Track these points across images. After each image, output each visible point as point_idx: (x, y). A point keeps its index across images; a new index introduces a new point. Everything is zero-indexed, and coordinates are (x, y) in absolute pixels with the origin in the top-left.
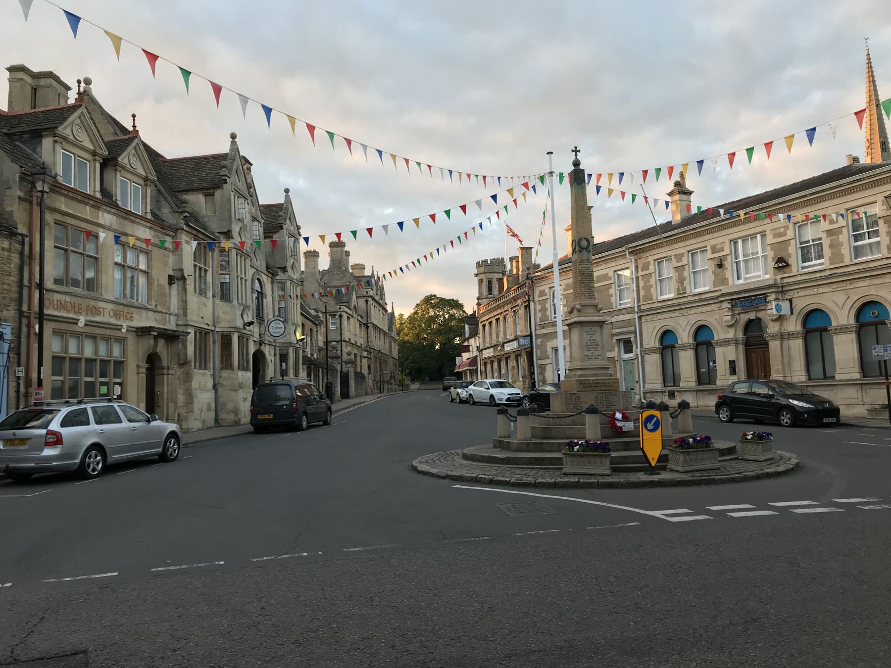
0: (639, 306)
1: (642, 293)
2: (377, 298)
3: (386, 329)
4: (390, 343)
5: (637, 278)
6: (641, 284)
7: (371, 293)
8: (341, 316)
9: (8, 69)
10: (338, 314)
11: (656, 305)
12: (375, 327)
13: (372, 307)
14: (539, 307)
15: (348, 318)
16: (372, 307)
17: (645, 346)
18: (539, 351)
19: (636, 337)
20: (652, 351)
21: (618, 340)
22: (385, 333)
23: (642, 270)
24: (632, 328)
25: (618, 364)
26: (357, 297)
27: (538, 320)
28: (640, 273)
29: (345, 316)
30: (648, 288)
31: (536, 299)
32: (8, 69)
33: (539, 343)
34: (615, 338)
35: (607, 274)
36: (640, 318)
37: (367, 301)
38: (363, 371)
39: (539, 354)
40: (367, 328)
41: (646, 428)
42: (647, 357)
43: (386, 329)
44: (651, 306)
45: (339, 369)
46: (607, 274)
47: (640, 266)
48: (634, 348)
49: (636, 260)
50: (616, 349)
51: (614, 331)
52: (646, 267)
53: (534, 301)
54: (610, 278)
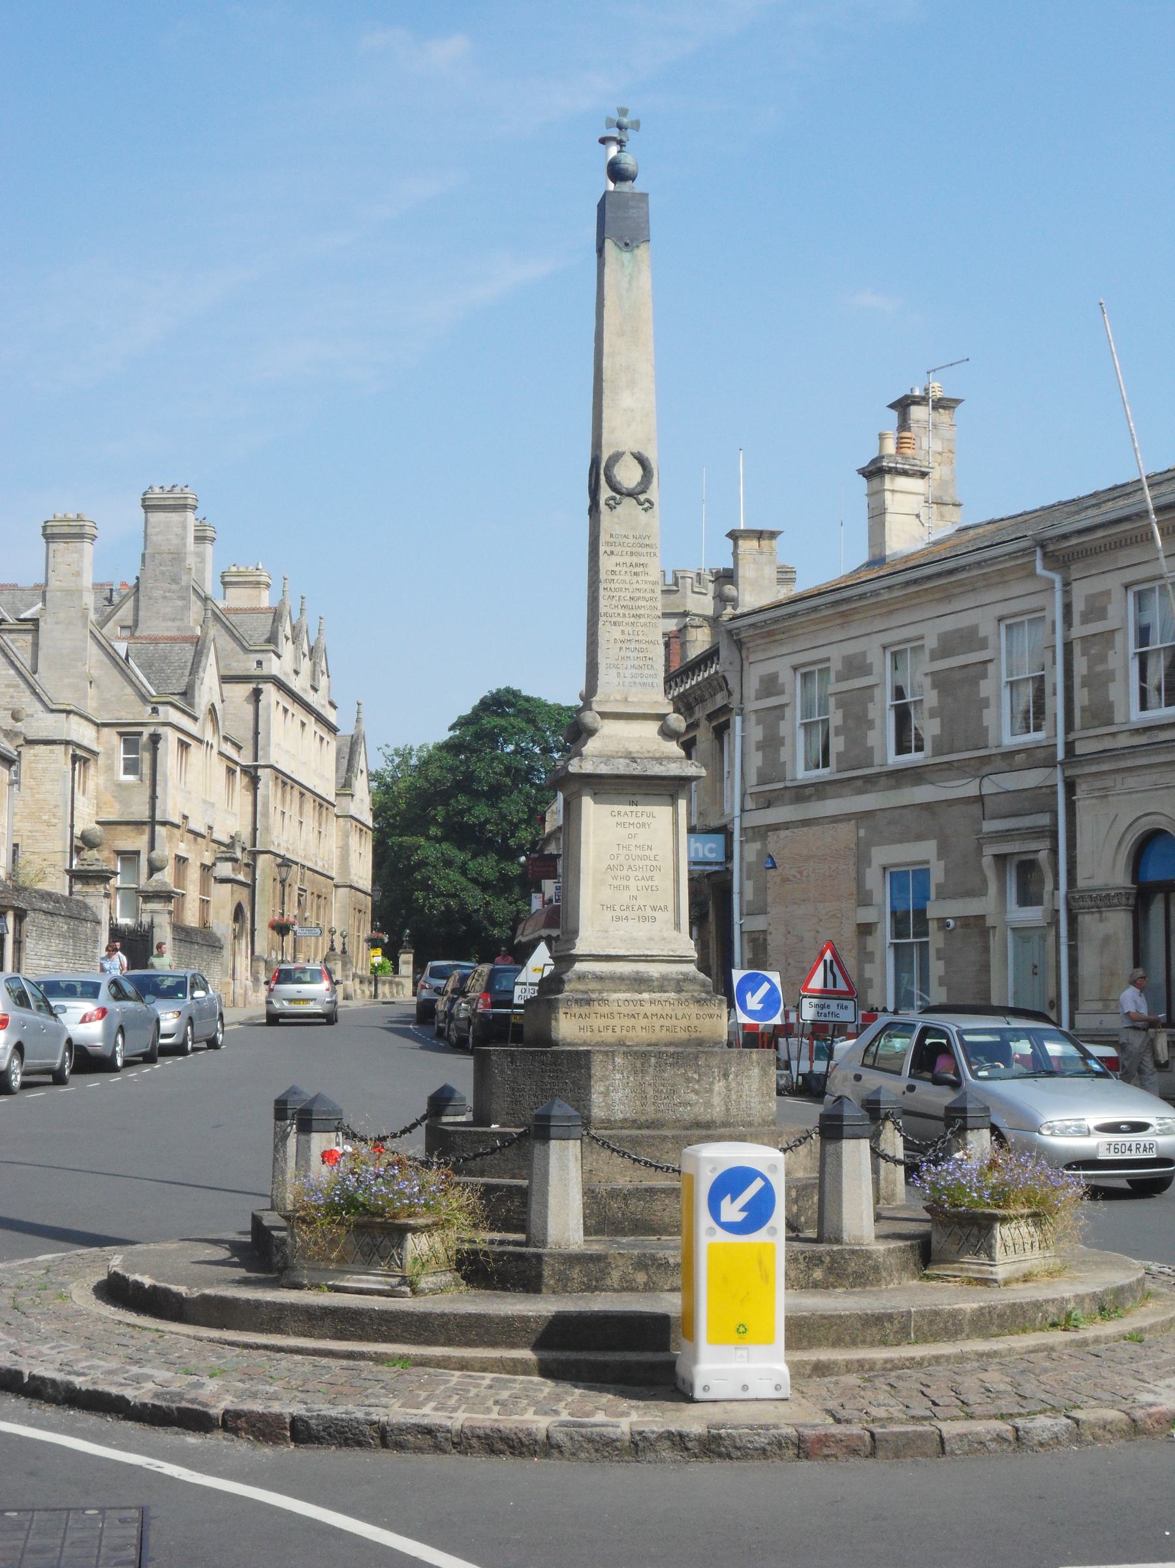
0: (1069, 747)
1: (1081, 697)
2: (298, 684)
3: (327, 788)
4: (346, 836)
5: (1068, 646)
6: (1081, 666)
7: (274, 666)
8: (155, 739)
9: (891, 406)
10: (147, 732)
11: (1123, 741)
12: (285, 780)
13: (277, 715)
14: (757, 733)
15: (184, 746)
16: (277, 715)
17: (1081, 883)
18: (749, 885)
19: (1054, 851)
20: (1102, 901)
21: (1001, 859)
22: (322, 803)
23: (1086, 619)
24: (1044, 820)
25: (994, 943)
26: (225, 679)
27: (753, 778)
28: (1078, 631)
29: (171, 738)
30: (1099, 681)
31: (752, 705)
32: (891, 406)
33: (751, 857)
34: (990, 850)
35: (974, 629)
36: (1070, 787)
37: (257, 693)
38: (213, 921)
39: (749, 895)
40: (254, 781)
41: (715, 1211)
42: (1087, 921)
43: (327, 788)
44: (1108, 744)
45: (104, 918)
46: (974, 629)
47: (1078, 607)
48: (1048, 886)
49: (1067, 584)
50: (993, 889)
51: (989, 826)
52: (1096, 611)
53: (741, 712)
54: (983, 644)
